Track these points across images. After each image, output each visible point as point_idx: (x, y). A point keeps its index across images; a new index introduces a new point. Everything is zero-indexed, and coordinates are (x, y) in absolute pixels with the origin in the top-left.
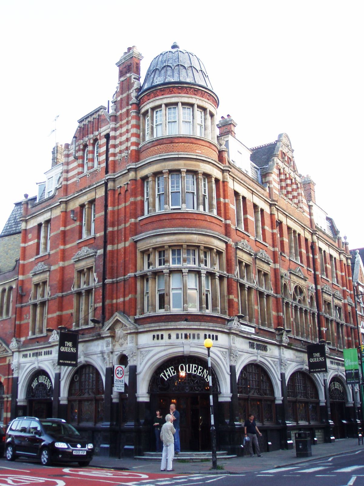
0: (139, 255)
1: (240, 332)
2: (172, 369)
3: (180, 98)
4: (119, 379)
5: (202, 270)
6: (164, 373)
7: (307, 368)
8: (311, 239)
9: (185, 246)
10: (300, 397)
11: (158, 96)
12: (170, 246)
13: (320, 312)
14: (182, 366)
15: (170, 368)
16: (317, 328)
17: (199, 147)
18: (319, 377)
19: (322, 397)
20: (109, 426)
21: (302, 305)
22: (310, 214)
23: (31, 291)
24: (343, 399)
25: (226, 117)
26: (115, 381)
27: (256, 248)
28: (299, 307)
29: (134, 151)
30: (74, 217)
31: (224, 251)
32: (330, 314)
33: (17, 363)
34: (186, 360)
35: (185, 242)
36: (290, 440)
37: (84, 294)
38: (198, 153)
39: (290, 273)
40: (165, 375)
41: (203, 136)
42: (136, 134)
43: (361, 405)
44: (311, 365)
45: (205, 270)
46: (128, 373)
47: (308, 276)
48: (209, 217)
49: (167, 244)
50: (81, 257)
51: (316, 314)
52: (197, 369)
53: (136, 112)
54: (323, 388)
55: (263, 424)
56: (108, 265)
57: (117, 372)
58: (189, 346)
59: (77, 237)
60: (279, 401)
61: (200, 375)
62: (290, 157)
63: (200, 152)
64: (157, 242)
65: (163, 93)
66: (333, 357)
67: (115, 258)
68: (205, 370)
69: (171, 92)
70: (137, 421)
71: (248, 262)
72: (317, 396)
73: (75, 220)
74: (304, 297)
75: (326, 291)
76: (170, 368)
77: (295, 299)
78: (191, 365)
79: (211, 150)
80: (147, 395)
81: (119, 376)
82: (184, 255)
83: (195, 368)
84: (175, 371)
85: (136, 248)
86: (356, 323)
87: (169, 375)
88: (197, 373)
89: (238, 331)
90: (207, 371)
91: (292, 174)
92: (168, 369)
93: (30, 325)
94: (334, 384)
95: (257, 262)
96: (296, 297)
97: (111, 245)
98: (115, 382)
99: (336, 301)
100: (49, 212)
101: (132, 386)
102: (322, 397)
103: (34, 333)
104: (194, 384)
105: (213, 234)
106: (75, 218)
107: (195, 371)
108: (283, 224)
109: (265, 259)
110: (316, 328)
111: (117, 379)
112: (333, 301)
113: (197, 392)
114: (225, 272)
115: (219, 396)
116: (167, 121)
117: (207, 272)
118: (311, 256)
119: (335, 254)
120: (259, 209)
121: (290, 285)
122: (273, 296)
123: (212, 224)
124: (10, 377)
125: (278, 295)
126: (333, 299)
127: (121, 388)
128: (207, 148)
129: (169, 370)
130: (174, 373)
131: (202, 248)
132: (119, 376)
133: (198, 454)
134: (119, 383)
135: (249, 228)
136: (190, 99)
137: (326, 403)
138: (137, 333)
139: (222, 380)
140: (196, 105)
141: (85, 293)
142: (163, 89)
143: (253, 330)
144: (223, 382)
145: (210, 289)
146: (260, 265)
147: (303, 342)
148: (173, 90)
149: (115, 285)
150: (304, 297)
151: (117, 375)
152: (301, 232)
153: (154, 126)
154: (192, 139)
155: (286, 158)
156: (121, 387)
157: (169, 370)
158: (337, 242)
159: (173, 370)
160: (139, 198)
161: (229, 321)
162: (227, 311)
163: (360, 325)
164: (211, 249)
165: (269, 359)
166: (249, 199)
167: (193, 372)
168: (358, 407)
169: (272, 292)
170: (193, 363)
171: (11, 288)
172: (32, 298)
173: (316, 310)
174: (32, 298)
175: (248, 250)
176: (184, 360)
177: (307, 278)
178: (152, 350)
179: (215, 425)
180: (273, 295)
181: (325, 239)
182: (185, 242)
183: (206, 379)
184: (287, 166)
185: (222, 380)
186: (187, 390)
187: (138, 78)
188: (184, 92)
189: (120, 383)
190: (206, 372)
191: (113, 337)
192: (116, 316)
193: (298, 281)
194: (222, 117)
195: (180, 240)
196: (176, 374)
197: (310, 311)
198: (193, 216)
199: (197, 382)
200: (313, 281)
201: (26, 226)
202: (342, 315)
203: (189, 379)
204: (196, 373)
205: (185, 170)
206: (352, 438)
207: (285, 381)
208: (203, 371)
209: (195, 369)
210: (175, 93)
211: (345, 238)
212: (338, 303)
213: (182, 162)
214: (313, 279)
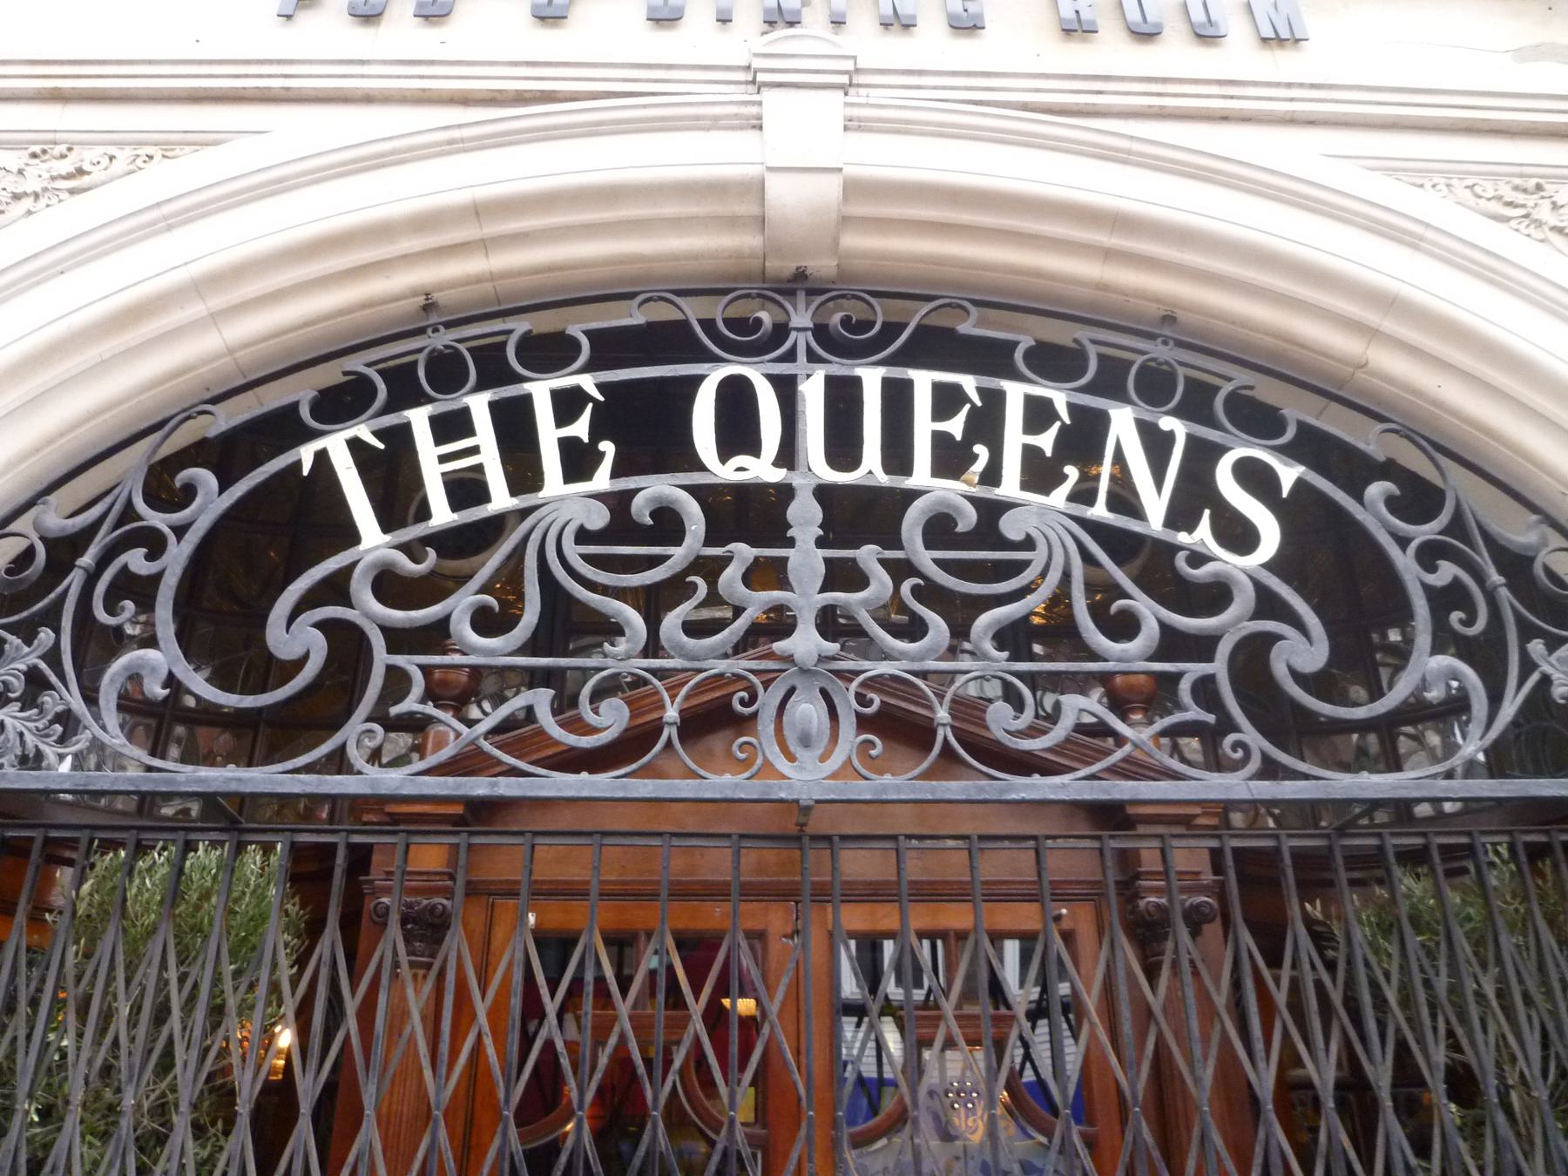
2: (567, 405)
6: (400, 438)
52: (987, 424)
68: (1123, 423)
78: (872, 378)
84: (608, 448)
88: (992, 475)
107: (950, 459)
159: (580, 428)
190: (1156, 445)
196: (602, 480)
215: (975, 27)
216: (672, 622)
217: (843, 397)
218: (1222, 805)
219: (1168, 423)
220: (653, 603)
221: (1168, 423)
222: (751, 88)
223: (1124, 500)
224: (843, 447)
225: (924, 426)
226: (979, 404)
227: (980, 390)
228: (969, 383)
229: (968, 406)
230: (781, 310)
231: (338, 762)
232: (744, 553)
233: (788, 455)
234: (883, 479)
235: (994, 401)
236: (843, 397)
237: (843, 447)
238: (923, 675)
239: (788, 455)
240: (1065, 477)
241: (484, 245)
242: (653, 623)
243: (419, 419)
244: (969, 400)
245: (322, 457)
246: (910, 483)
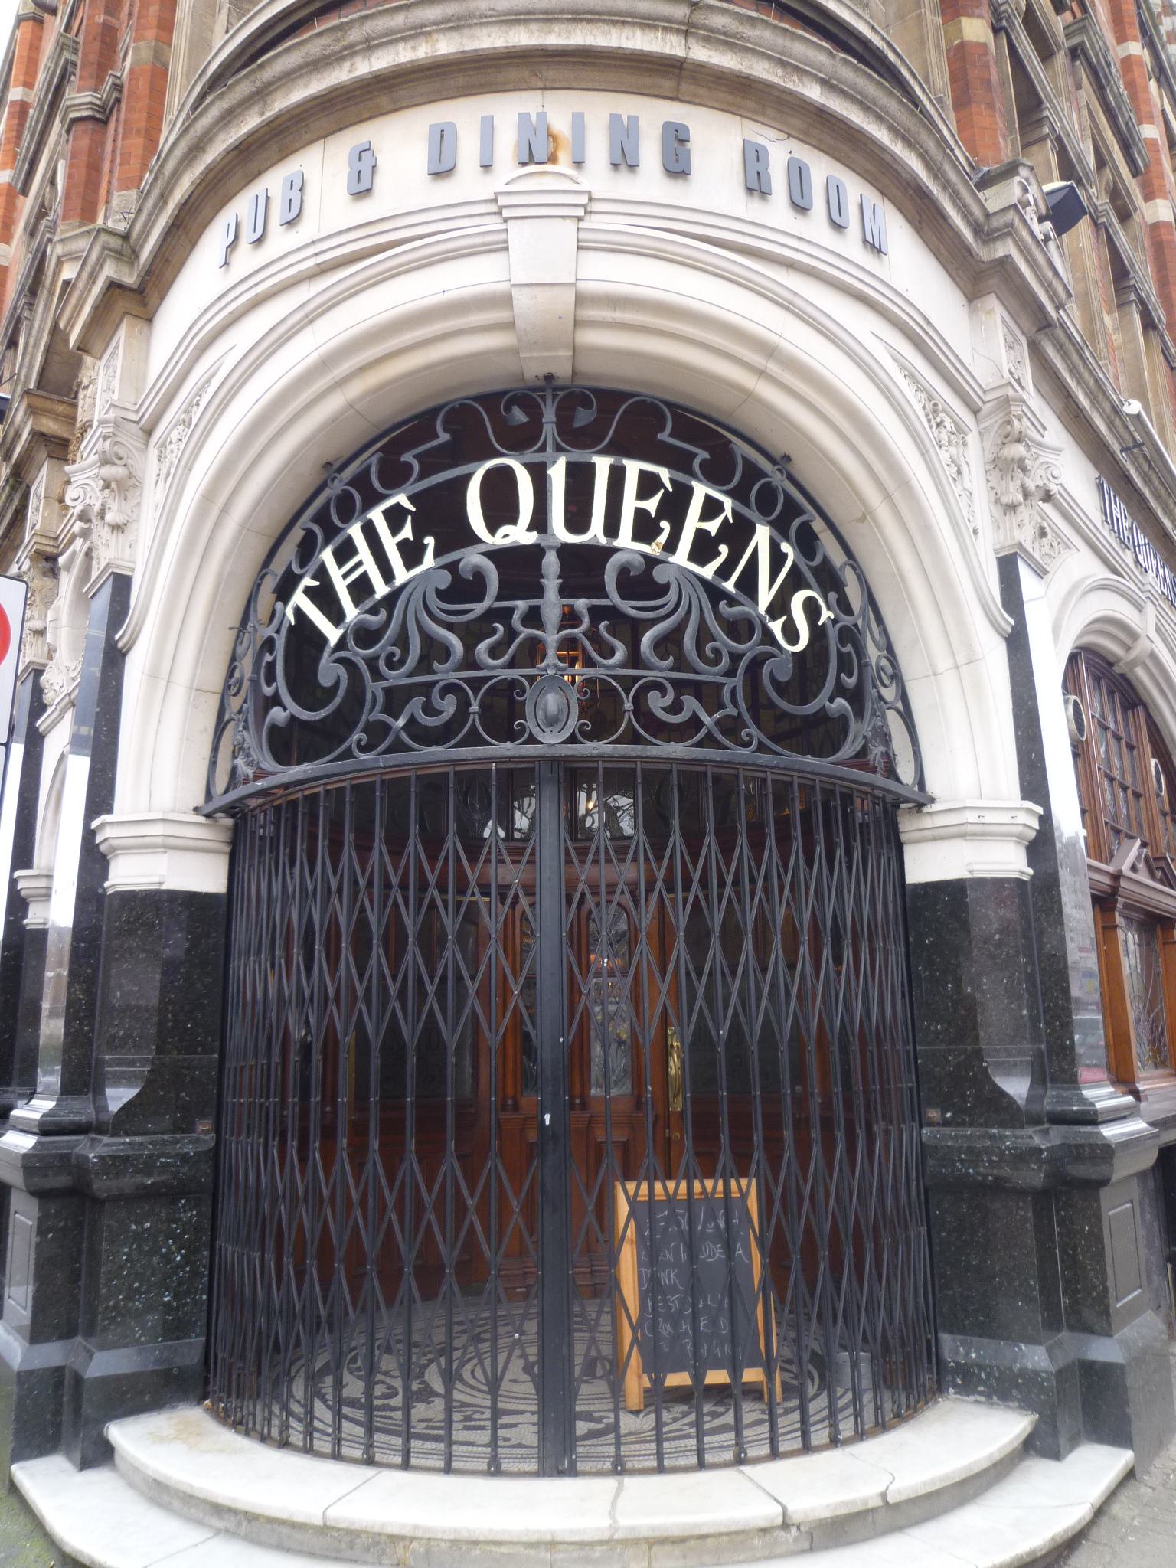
2: (395, 518)
6: (322, 573)
14: (507, 473)
15: (376, 515)
40: (323, 595)
52: (675, 506)
68: (762, 535)
76: (376, 515)
78: (602, 464)
83: (644, 493)
84: (430, 541)
87: (361, 588)
88: (671, 546)
92: (355, 531)
104: (635, 659)
107: (645, 528)
115: (908, 826)
129: (369, 531)
130: (411, 553)
139: (9, 1333)
144: (949, 682)
157: (369, 531)
159: (407, 532)
167: (625, 538)
170: (620, 448)
176: (519, 416)
185: (943, 663)
196: (429, 560)
199: (669, 644)
203: (581, 604)
204: (653, 549)
206: (211, 1416)
208: (738, 533)
216: (483, 647)
217: (580, 480)
218: (530, 1316)
220: (471, 634)
221: (785, 547)
222: (497, 219)
223: (748, 584)
224: (578, 520)
225: (630, 503)
226: (671, 490)
227: (672, 481)
229: (662, 491)
231: (348, 755)
232: (521, 605)
233: (540, 522)
234: (603, 541)
236: (580, 480)
237: (578, 520)
238: (615, 677)
239: (540, 522)
240: (719, 554)
242: (470, 648)
244: (664, 487)
245: (299, 612)
246: (617, 543)
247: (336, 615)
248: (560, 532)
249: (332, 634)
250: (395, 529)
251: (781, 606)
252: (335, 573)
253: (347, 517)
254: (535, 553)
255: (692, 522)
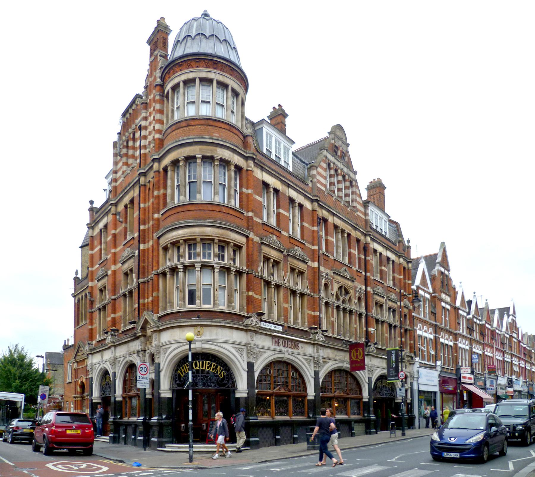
0: (161, 252)
1: (260, 329)
3: (198, 73)
4: (143, 376)
5: (215, 265)
6: (181, 369)
7: (349, 366)
8: (364, 240)
9: (198, 240)
10: (339, 393)
11: (177, 72)
12: (185, 241)
13: (369, 313)
15: (186, 365)
16: (365, 329)
17: (216, 129)
18: (363, 376)
19: (365, 394)
20: (156, 421)
21: (347, 306)
22: (366, 214)
23: (97, 296)
24: (392, 396)
25: (277, 107)
26: (138, 377)
27: (290, 245)
28: (342, 307)
29: (158, 140)
30: (120, 219)
31: (244, 245)
32: (382, 315)
33: (28, 361)
34: (200, 357)
35: (199, 236)
36: (296, 434)
37: (127, 296)
38: (216, 136)
39: (334, 273)
40: (181, 371)
41: (224, 118)
42: (159, 120)
43: (411, 401)
44: (352, 362)
45: (218, 264)
46: (154, 371)
47: (356, 277)
48: (225, 208)
49: (182, 238)
50: (125, 259)
51: (364, 315)
52: (211, 366)
53: (160, 95)
54: (367, 386)
55: (273, 419)
56: (142, 264)
57: (140, 369)
58: (201, 343)
59: (123, 239)
60: (365, 400)
61: (213, 371)
62: (345, 152)
63: (217, 135)
64: (173, 236)
65: (180, 68)
66: (380, 356)
67: (146, 258)
69: (189, 66)
70: (160, 415)
71: (277, 258)
72: (361, 392)
73: (122, 222)
74: (350, 298)
75: (378, 293)
77: (338, 299)
78: (205, 362)
79: (232, 134)
80: (169, 391)
81: (143, 373)
82: (199, 249)
85: (158, 244)
86: (412, 324)
89: (257, 328)
90: (221, 368)
91: (345, 170)
93: (98, 328)
94: (382, 382)
95: (289, 259)
96: (340, 297)
97: (143, 244)
98: (138, 379)
99: (390, 303)
100: (105, 217)
101: (155, 384)
102: (365, 394)
103: (100, 336)
104: (207, 380)
105: (228, 226)
106: (121, 220)
107: (208, 368)
108: (328, 222)
109: (300, 256)
110: (362, 328)
111: (141, 376)
112: (386, 303)
113: (210, 388)
114: (245, 268)
115: (236, 391)
116: (186, 101)
117: (221, 267)
118: (363, 257)
119: (393, 257)
120: (297, 204)
121: (332, 285)
122: (309, 295)
123: (229, 216)
124: (88, 377)
125: (315, 294)
126: (386, 300)
127: (146, 385)
128: (226, 131)
129: (185, 366)
131: (217, 241)
132: (143, 373)
133: (179, 447)
134: (143, 380)
135: (281, 222)
136: (209, 73)
137: (369, 399)
138: (160, 331)
140: (216, 82)
141: (128, 294)
142: (180, 64)
143: (280, 329)
144: (239, 378)
145: (226, 285)
146: (293, 263)
147: (344, 341)
148: (190, 64)
149: (146, 284)
150: (350, 298)
151: (141, 372)
152: (351, 231)
153: (175, 109)
154: (209, 121)
155: (339, 153)
156: (145, 383)
158: (398, 245)
160: (162, 191)
161: (247, 318)
162: (245, 308)
163: (417, 327)
164: (228, 243)
165: (300, 357)
166: (284, 193)
168: (408, 403)
169: (307, 291)
171: (86, 295)
172: (98, 303)
173: (363, 310)
174: (98, 303)
175: (277, 246)
177: (355, 279)
178: (170, 347)
179: (192, 421)
180: (309, 294)
181: (381, 241)
182: (199, 236)
183: (220, 376)
184: (339, 161)
185: (238, 376)
186: (200, 386)
187: (164, 55)
188: (202, 65)
189: (144, 380)
190: (220, 369)
191: (145, 336)
192: (145, 315)
193: (343, 282)
194: (274, 108)
195: (194, 233)
197: (356, 312)
198: (207, 207)
199: (210, 379)
200: (364, 283)
201: (93, 234)
202: (397, 317)
205: (200, 156)
207: (319, 378)
208: (216, 367)
209: (209, 365)
210: (192, 67)
211: (409, 241)
212: (392, 305)
213: (197, 148)
214: (363, 280)
215: (370, 196)
217: (203, 363)
219: (221, 368)
224: (202, 367)
225: (207, 365)
228: (210, 362)
230: (207, 470)
233: (199, 367)
235: (212, 364)
236: (203, 363)
237: (202, 367)
239: (199, 367)
241: (179, 224)
243: (181, 368)
247: (182, 374)
248: (201, 368)
249: (182, 376)
250: (214, 366)
251: (220, 373)
252: (182, 370)
253: (183, 364)
254: (199, 370)
255: (212, 367)
